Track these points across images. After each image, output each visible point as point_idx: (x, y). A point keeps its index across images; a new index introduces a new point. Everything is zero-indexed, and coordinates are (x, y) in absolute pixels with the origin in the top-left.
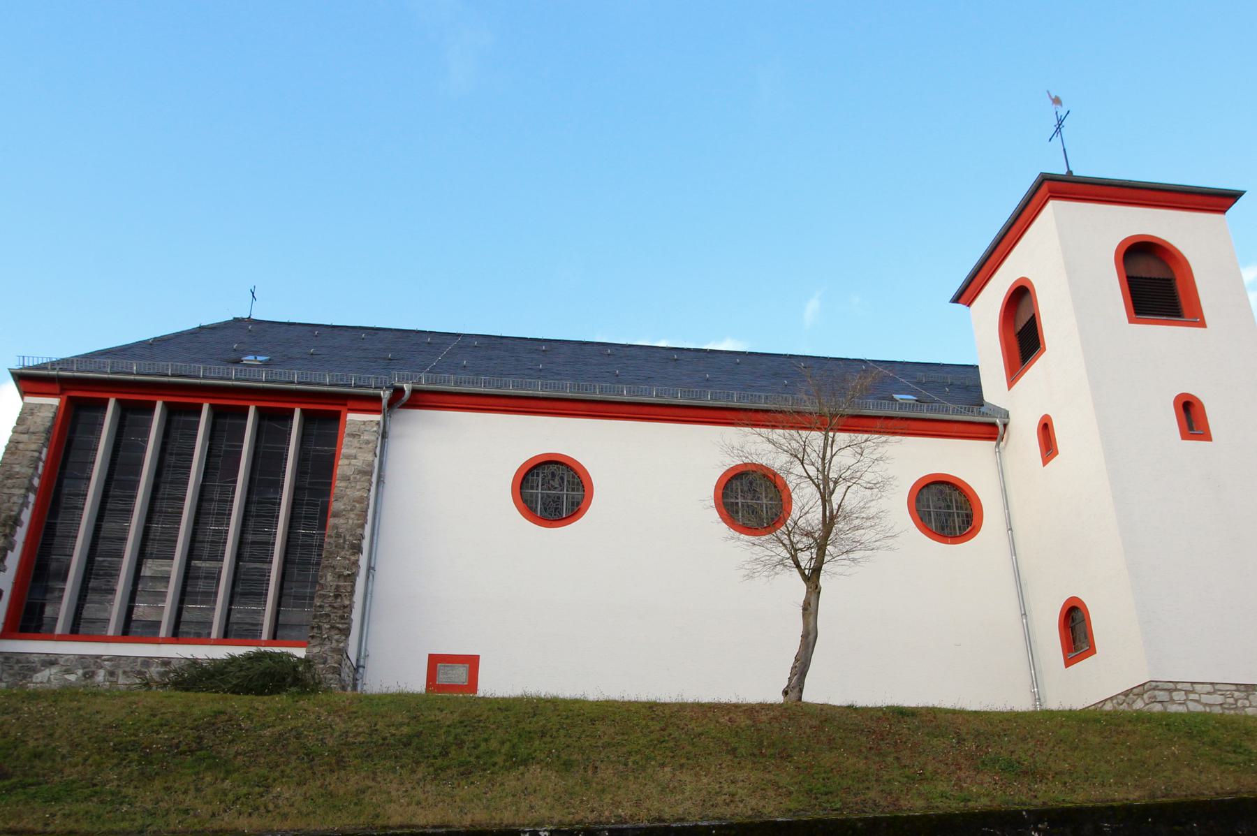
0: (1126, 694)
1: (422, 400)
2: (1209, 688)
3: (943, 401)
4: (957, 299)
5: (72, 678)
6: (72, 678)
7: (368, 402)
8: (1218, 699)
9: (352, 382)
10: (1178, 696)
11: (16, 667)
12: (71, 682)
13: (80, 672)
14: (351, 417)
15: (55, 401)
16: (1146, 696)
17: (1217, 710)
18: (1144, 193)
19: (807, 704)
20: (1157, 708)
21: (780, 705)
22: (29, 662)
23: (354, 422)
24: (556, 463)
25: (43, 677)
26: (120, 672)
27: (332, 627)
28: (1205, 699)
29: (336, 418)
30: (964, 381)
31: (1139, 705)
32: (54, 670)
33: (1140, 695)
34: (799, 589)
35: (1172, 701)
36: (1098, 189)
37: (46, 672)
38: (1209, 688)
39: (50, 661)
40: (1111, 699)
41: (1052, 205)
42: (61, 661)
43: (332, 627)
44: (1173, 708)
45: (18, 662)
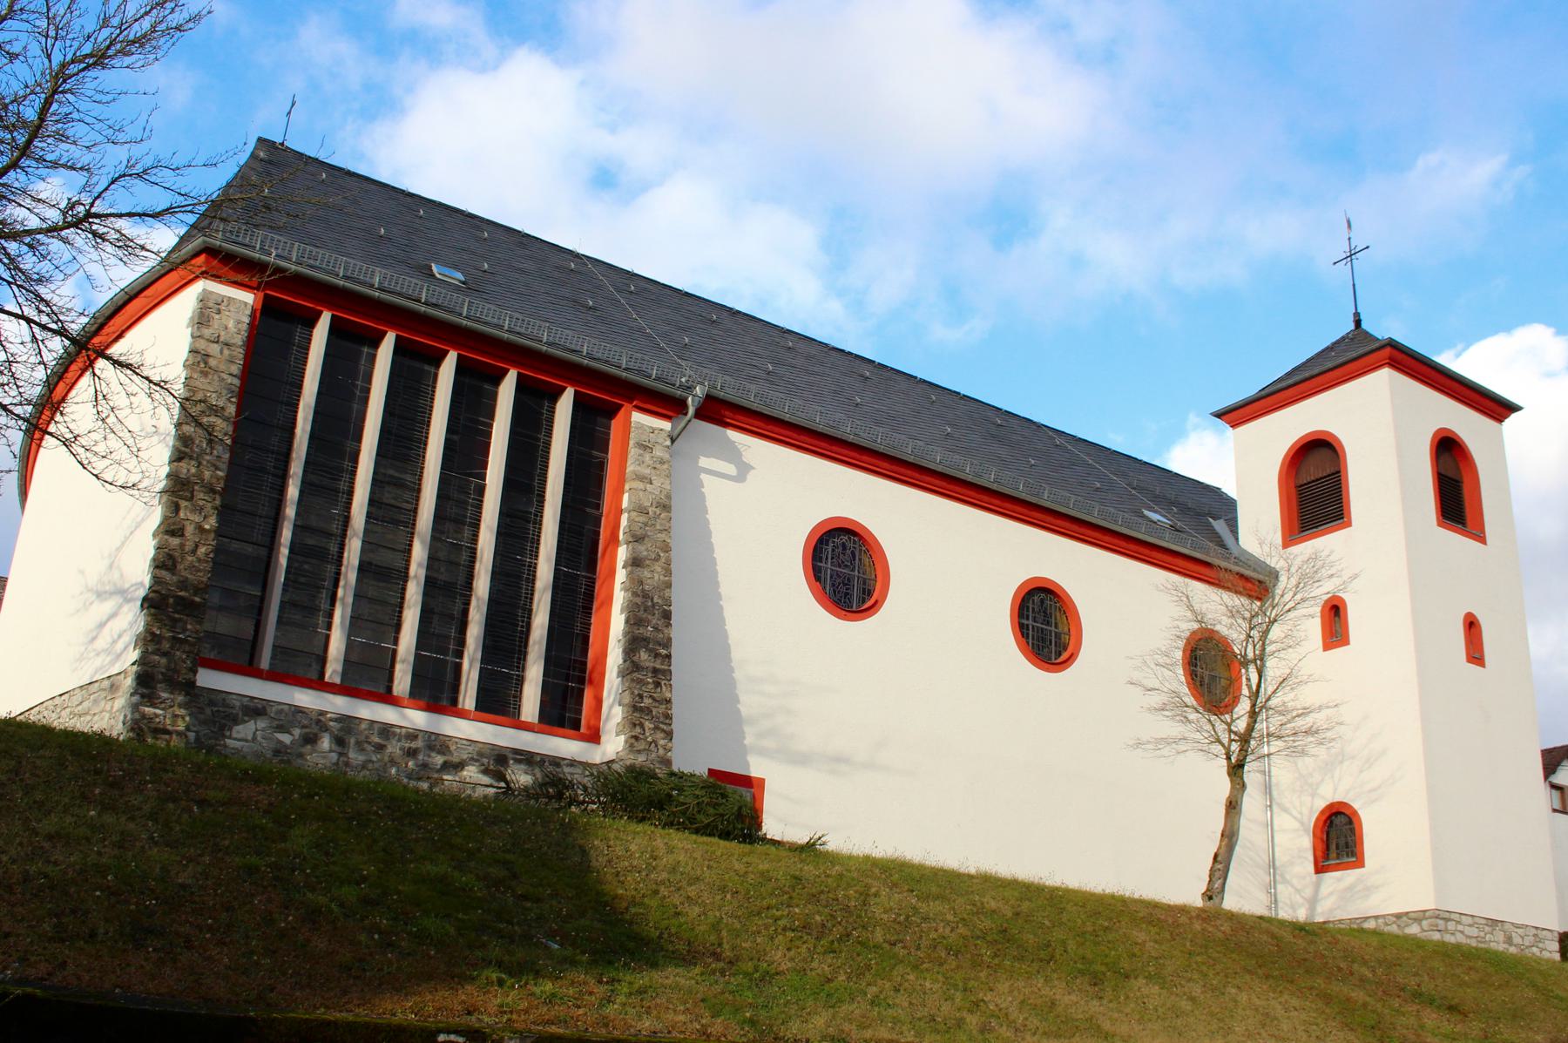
0: (1398, 916)
1: (717, 411)
2: (1470, 920)
3: (1171, 525)
4: (1220, 415)
5: (286, 738)
6: (286, 738)
7: (667, 404)
8: (1474, 932)
9: (653, 370)
10: (1451, 925)
11: (208, 711)
12: (286, 746)
13: (297, 732)
14: (638, 417)
15: (248, 297)
16: (1425, 923)
17: (1474, 943)
18: (1424, 368)
19: (1231, 916)
20: (1436, 936)
21: (1202, 910)
22: (228, 706)
23: (641, 427)
24: (855, 534)
25: (245, 736)
26: (352, 741)
27: (656, 728)
28: (1468, 931)
29: (612, 411)
30: (1206, 508)
31: (1414, 930)
32: (262, 723)
33: (1418, 920)
34: (1224, 786)
35: (1446, 930)
36: (1462, 389)
37: (251, 725)
38: (1470, 920)
39: (256, 709)
40: (1376, 917)
41: (1385, 374)
42: (272, 711)
43: (656, 728)
44: (1449, 938)
45: (212, 703)
